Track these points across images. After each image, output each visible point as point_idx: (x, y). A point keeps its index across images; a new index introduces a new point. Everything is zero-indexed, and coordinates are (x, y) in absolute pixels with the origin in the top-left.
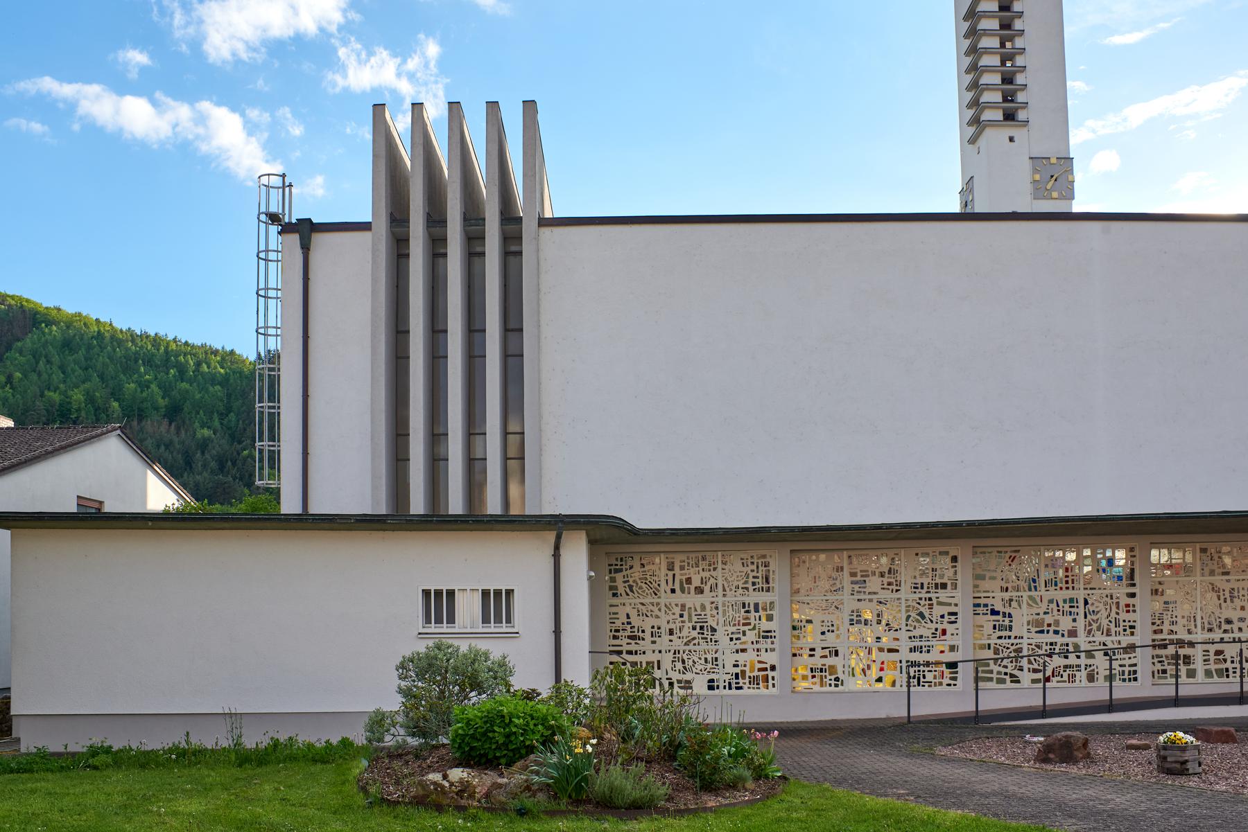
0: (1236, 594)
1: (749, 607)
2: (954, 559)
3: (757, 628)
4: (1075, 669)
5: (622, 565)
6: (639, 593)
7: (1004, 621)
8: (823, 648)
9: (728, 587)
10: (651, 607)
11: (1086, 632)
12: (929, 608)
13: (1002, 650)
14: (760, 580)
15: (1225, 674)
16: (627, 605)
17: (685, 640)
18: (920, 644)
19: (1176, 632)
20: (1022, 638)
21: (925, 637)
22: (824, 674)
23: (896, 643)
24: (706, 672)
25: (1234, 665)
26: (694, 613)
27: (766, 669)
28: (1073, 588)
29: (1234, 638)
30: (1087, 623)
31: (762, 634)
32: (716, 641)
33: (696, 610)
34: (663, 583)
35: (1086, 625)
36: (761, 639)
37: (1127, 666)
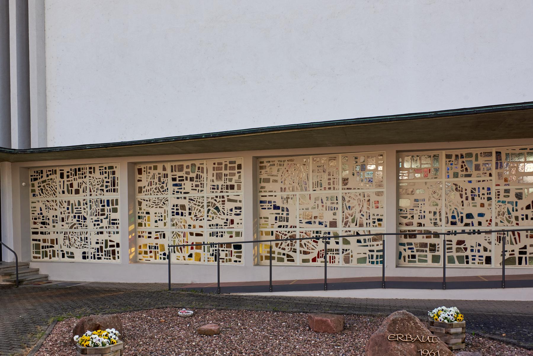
0: (477, 193)
1: (104, 203)
2: (239, 167)
3: (109, 217)
4: (335, 252)
5: (37, 176)
6: (46, 194)
7: (282, 214)
8: (156, 232)
9: (93, 189)
10: (52, 203)
11: (344, 223)
12: (222, 204)
13: (282, 236)
14: (109, 184)
15: (465, 260)
16: (40, 201)
17: (70, 225)
18: (216, 230)
19: (424, 225)
20: (296, 227)
21: (220, 225)
22: (157, 250)
23: (201, 229)
24: (81, 247)
25: (473, 254)
26: (74, 207)
27: (113, 246)
28: (334, 188)
29: (474, 231)
30: (344, 216)
31: (111, 221)
32: (86, 226)
33: (75, 205)
34: (58, 187)
35: (343, 217)
36: (111, 225)
37: (375, 251)
